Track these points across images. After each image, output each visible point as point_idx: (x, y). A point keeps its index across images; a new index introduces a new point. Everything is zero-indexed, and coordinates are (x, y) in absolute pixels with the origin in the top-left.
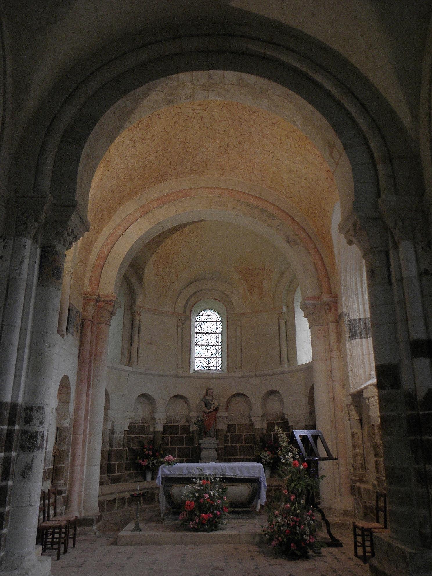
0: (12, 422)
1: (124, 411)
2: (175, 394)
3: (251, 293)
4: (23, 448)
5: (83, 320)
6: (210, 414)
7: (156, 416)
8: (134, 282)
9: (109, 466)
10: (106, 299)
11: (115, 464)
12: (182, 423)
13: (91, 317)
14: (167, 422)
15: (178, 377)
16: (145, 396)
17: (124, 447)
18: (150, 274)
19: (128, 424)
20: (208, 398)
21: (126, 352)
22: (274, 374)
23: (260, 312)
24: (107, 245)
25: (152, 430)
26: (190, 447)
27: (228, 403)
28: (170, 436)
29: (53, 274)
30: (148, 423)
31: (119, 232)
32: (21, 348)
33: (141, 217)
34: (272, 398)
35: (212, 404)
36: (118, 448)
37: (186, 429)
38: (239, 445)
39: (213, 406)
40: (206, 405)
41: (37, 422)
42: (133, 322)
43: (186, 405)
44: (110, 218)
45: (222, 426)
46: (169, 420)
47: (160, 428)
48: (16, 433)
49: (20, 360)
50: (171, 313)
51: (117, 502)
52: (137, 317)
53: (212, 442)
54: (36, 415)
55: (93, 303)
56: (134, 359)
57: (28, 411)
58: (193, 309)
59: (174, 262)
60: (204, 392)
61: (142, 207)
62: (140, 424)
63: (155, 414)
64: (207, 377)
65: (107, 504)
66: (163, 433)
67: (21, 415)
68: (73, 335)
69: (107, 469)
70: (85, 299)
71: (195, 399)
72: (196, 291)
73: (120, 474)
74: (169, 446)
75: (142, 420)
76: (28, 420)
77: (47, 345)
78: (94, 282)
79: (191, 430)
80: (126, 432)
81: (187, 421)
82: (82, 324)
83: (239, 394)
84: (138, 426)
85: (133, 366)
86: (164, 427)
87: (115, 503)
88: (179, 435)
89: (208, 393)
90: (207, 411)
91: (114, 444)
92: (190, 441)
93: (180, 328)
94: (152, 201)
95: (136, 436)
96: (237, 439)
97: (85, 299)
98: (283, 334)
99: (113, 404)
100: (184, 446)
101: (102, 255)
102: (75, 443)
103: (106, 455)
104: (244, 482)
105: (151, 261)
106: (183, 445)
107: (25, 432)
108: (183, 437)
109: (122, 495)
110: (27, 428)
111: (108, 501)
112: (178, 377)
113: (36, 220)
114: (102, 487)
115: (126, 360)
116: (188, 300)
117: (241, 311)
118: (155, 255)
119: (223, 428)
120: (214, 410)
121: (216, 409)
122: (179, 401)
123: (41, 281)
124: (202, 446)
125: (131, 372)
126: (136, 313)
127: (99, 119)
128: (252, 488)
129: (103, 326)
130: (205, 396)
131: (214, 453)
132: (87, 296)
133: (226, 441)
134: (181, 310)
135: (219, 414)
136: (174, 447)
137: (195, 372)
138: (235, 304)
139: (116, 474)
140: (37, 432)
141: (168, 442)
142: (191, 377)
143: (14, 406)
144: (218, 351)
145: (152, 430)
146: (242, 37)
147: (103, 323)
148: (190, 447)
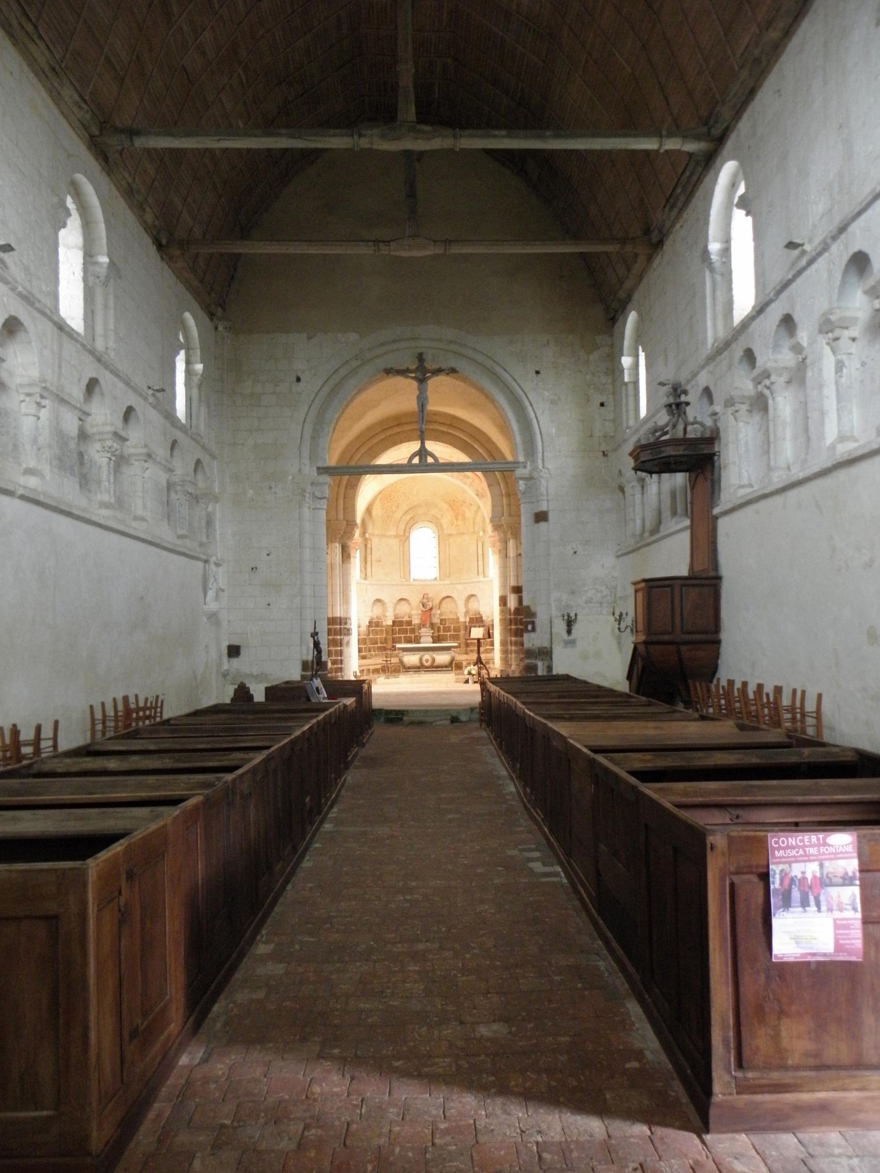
3: (457, 519)
7: (387, 614)
12: (406, 619)
16: (378, 601)
20: (425, 600)
22: (473, 583)
23: (463, 534)
25: (384, 624)
27: (440, 603)
34: (472, 599)
37: (409, 623)
38: (449, 633)
42: (366, 545)
45: (436, 620)
46: (396, 616)
47: (390, 623)
56: (369, 574)
67: (343, 621)
71: (415, 600)
76: (346, 623)
81: (409, 617)
83: (448, 597)
86: (394, 622)
92: (413, 631)
96: (447, 629)
98: (480, 553)
115: (363, 576)
117: (449, 532)
121: (431, 609)
122: (403, 602)
131: (799, 904)
133: (439, 631)
134: (402, 533)
135: (433, 612)
138: (444, 526)
143: (340, 618)
145: (384, 624)
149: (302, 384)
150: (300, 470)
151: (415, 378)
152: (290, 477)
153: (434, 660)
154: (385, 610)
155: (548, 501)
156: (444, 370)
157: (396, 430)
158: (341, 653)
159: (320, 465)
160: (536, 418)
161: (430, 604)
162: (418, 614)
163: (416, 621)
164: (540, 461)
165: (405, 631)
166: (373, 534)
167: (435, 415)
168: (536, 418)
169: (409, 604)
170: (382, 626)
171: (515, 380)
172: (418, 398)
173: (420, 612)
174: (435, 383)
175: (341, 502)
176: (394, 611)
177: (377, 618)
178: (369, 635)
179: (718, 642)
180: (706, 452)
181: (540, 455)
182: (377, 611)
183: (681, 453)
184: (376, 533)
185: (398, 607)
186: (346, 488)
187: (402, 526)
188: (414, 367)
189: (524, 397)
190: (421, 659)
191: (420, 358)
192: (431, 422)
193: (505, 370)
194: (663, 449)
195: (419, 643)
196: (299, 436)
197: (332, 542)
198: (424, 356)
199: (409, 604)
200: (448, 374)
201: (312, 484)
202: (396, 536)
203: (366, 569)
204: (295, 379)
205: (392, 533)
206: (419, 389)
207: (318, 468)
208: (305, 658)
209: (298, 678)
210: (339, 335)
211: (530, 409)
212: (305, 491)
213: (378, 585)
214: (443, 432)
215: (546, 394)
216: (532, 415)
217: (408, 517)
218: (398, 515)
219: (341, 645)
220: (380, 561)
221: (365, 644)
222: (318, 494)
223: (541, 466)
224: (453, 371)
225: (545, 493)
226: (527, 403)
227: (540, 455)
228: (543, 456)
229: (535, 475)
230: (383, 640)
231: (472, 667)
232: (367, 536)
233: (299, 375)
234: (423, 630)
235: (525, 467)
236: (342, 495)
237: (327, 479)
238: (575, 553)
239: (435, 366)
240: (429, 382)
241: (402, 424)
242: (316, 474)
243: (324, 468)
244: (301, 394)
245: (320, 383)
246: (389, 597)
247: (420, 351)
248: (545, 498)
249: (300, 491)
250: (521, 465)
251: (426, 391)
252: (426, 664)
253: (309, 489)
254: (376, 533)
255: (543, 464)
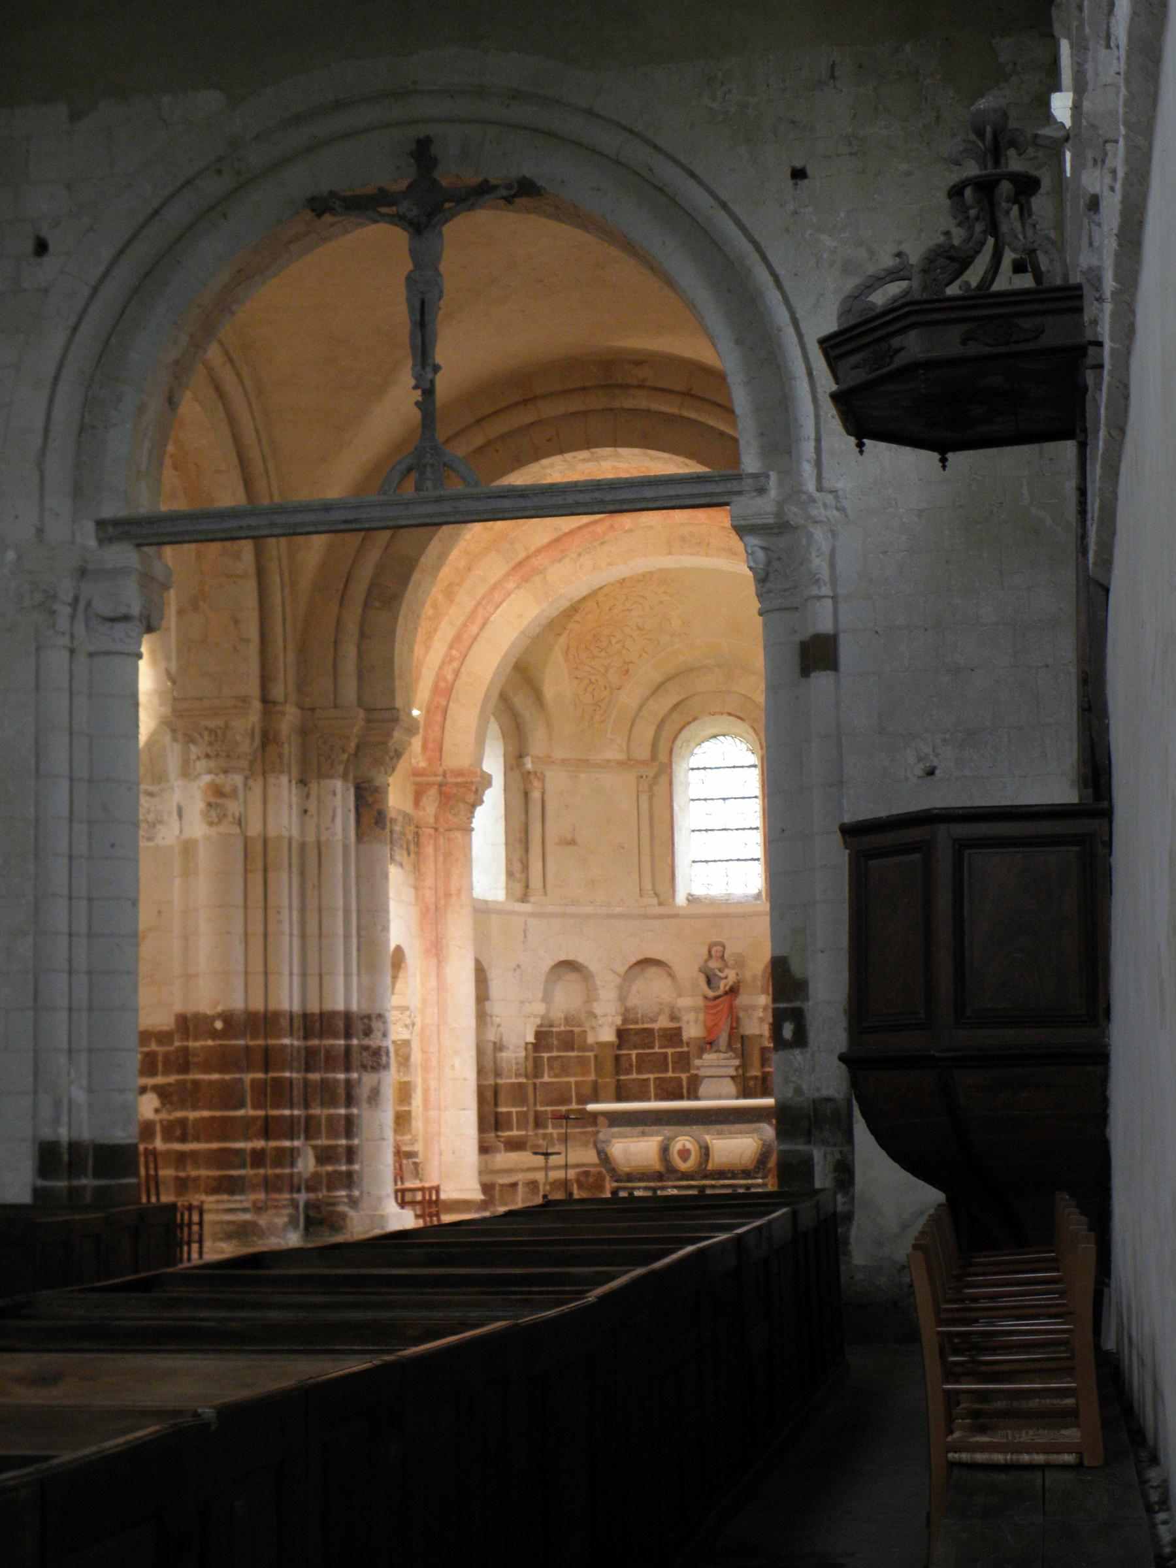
0: (348, 1035)
1: (522, 1002)
2: (640, 957)
4: (364, 1067)
5: (417, 827)
6: (718, 1001)
7: (598, 1008)
8: (521, 701)
9: (497, 1115)
10: (460, 780)
11: (510, 1113)
12: (663, 1022)
13: (432, 821)
14: (625, 1021)
15: (646, 917)
16: (570, 966)
17: (526, 1076)
18: (557, 683)
19: (534, 1029)
20: (713, 964)
21: (517, 867)
24: (452, 660)
25: (591, 1040)
26: (684, 1076)
28: (634, 1053)
29: (376, 823)
30: (579, 1026)
31: (474, 629)
32: (347, 937)
33: (518, 587)
35: (722, 979)
36: (514, 1080)
39: (722, 984)
40: (709, 982)
41: (377, 1034)
42: (526, 794)
43: (668, 981)
44: (452, 601)
46: (627, 1015)
47: (607, 1035)
48: (354, 1050)
49: (347, 953)
50: (621, 764)
51: (520, 1188)
52: (536, 783)
53: (725, 1062)
54: (376, 1025)
55: (433, 792)
56: (536, 882)
57: (366, 1021)
58: (678, 743)
59: (614, 641)
60: (705, 951)
61: (519, 565)
62: (563, 1028)
63: (595, 1005)
64: (716, 913)
65: (501, 1191)
66: (620, 1047)
67: (359, 1026)
68: (401, 865)
69: (491, 1122)
70: (416, 784)
71: (687, 963)
72: (680, 698)
73: (523, 1133)
74: (634, 1076)
75: (566, 1019)
76: (368, 1032)
77: (380, 928)
78: (431, 745)
79: (685, 1036)
80: (530, 1046)
81: (673, 1018)
82: (417, 834)
84: (559, 1033)
85: (532, 899)
86: (620, 1033)
87: (516, 1191)
88: (657, 1050)
89: (713, 953)
90: (711, 994)
91: (505, 1072)
92: (683, 1061)
93: (644, 798)
94: (538, 551)
95: (555, 1054)
97: (416, 784)
99: (496, 989)
100: (670, 1074)
101: (442, 684)
102: (426, 1069)
103: (489, 1095)
104: (718, 1122)
105: (558, 651)
106: (666, 1070)
107: (366, 1048)
108: (665, 1055)
109: (531, 1176)
110: (366, 1042)
111: (502, 1186)
112: (646, 917)
113: (344, 751)
114: (486, 1157)
115: (518, 888)
116: (660, 726)
118: (566, 633)
119: (757, 1032)
120: (726, 993)
122: (652, 971)
123: (359, 838)
124: (702, 1072)
125: (532, 915)
126: (532, 777)
127: (417, 561)
128: (760, 1143)
129: (458, 835)
130: (707, 961)
132: (420, 779)
134: (643, 753)
135: (743, 1000)
136: (645, 1076)
137: (692, 899)
139: (515, 1133)
140: (380, 1048)
141: (631, 1065)
142: (676, 916)
143: (348, 1016)
144: (754, 844)
145: (591, 1040)
146: (641, 387)
147: (457, 829)
148: (684, 1076)
149: (50, 262)
150: (40, 531)
151: (399, 220)
152: (11, 555)
153: (706, 1151)
154: (591, 996)
155: (834, 598)
156: (496, 187)
157: (525, 417)
158: (349, 1126)
159: (111, 510)
160: (795, 323)
161: (731, 976)
162: (695, 1009)
163: (692, 1030)
164: (808, 469)
165: (661, 1063)
166: (549, 761)
167: (638, 363)
168: (795, 323)
169: (671, 975)
170: (584, 1047)
171: (724, 206)
172: (410, 280)
173: (700, 1002)
174: (475, 241)
175: (350, 651)
176: (622, 998)
177: (568, 1020)
178: (537, 1070)
179: (1100, 1058)
180: (1048, 340)
181: (808, 448)
182: (566, 1000)
183: (956, 350)
184: (558, 754)
185: (638, 986)
186: (366, 605)
187: (645, 733)
188: (403, 185)
189: (753, 258)
190: (665, 1150)
191: (423, 153)
192: (625, 387)
193: (693, 175)
194: (896, 342)
195: (697, 1098)
196: (39, 424)
197: (322, 776)
198: (434, 150)
199: (671, 975)
200: (509, 200)
201: (82, 573)
202: (623, 765)
203: (525, 867)
204: (29, 246)
205: (613, 753)
206: (413, 252)
207: (101, 524)
208: (46, 1133)
209: (26, 1198)
210: (166, 99)
211: (773, 297)
212: (55, 597)
213: (564, 915)
214: (669, 419)
215: (828, 241)
216: (781, 316)
217: (664, 703)
218: (629, 697)
219: (350, 1101)
220: (573, 842)
221: (523, 1101)
222: (103, 607)
223: (811, 486)
224: (524, 190)
225: (825, 574)
226: (762, 275)
227: (808, 448)
228: (818, 450)
229: (793, 513)
230: (587, 1091)
231: (593, 1077)
232: (529, 765)
233: (44, 232)
234: (709, 1057)
235: (762, 491)
236: (352, 629)
237: (123, 555)
238: (931, 772)
239: (471, 178)
240: (447, 229)
241: (535, 398)
242: (92, 543)
243: (116, 523)
244: (46, 291)
245: (106, 255)
246: (603, 956)
247: (422, 131)
248: (826, 590)
249: (39, 597)
250: (747, 483)
251: (438, 258)
252: (683, 1166)
253: (66, 588)
254: (558, 754)
255: (819, 477)
